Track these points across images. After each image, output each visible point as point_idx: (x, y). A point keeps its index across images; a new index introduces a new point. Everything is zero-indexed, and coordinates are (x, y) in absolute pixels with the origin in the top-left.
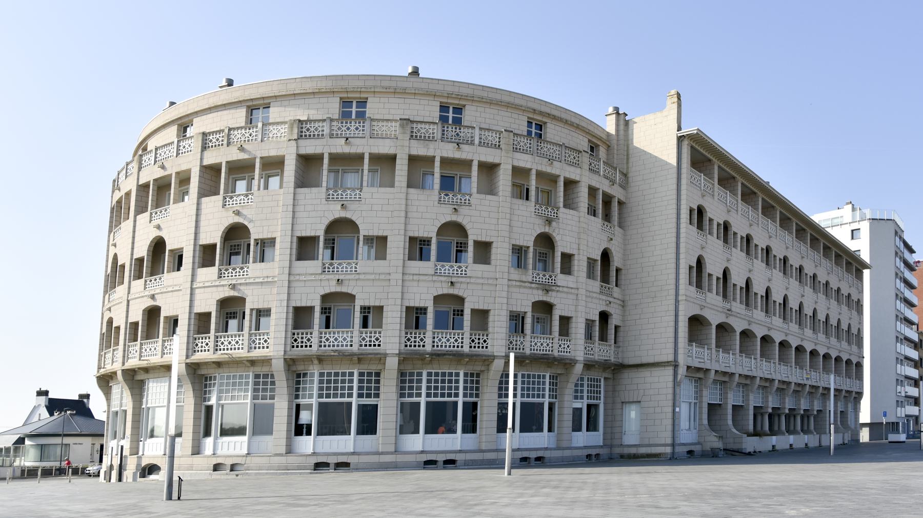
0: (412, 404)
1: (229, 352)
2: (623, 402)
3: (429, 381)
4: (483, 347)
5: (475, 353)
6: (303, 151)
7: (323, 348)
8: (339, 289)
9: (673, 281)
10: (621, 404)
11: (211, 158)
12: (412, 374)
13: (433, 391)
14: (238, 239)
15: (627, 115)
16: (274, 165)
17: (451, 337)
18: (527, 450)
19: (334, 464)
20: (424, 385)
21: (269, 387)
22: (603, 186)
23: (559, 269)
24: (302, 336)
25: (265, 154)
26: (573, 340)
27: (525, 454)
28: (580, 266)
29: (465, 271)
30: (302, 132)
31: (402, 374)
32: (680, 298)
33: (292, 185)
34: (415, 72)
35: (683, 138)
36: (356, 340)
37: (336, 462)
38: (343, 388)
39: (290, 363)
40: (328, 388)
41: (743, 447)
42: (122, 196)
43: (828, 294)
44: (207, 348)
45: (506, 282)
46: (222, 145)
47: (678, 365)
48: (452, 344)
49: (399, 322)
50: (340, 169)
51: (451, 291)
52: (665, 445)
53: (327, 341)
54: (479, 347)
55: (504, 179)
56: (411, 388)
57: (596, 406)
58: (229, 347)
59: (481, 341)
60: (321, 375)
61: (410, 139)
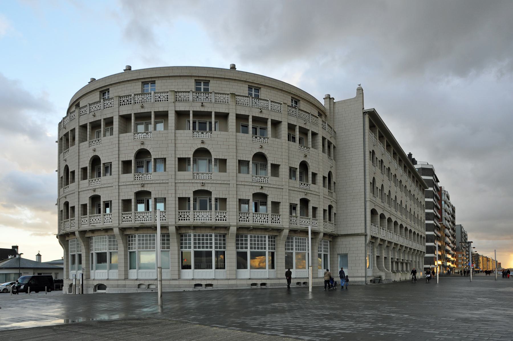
0: (207, 252)
1: (143, 222)
2: (338, 254)
3: (195, 240)
4: (246, 221)
5: (257, 225)
6: (178, 109)
7: (196, 221)
8: (203, 188)
9: (363, 190)
10: (337, 255)
11: (125, 110)
12: (242, 237)
13: (197, 245)
14: (142, 158)
15: (334, 99)
16: (162, 116)
17: (262, 217)
18: (299, 278)
19: (205, 285)
20: (249, 242)
21: (240, 242)
22: (328, 138)
23: (311, 182)
24: (184, 214)
25: (157, 110)
26: (318, 220)
27: (299, 281)
28: (319, 179)
29: (267, 180)
30: (176, 98)
31: (237, 236)
32: (367, 200)
33: (173, 128)
34: (233, 67)
35: (366, 113)
36: (213, 217)
37: (206, 284)
38: (207, 243)
39: (178, 228)
40: (199, 243)
41: (391, 279)
42: (68, 132)
43: (382, 198)
44: (130, 220)
45: (287, 187)
46: (131, 103)
47: (367, 235)
48: (263, 221)
49: (236, 207)
50: (144, 123)
51: (261, 191)
52: (362, 277)
53: (197, 216)
54: (244, 221)
55: (284, 130)
56: (242, 244)
57: (327, 255)
58: (143, 219)
59: (245, 217)
60: (195, 236)
61: (236, 105)
